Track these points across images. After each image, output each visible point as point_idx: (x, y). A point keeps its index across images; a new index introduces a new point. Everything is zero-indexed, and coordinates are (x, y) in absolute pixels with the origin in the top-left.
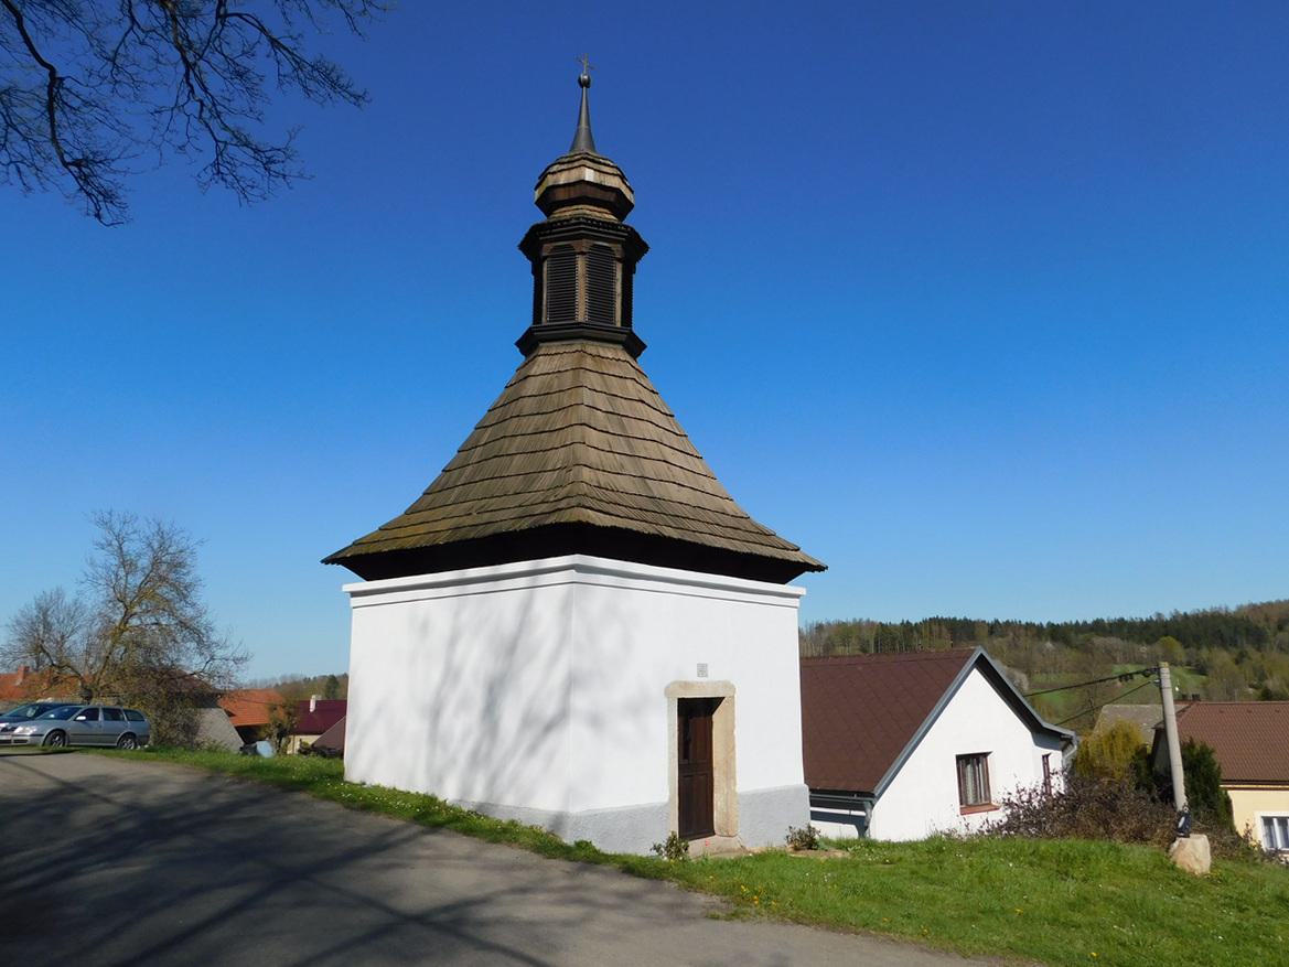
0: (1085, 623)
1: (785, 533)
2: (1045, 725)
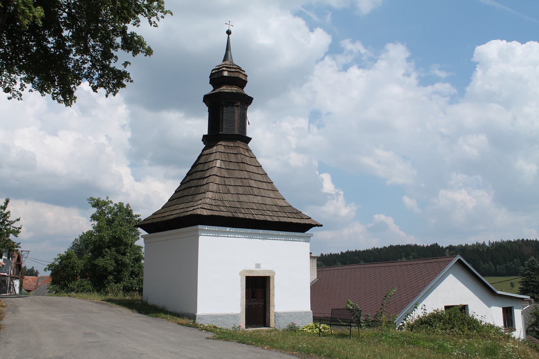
0: (442, 247)
1: (306, 212)
2: (499, 292)
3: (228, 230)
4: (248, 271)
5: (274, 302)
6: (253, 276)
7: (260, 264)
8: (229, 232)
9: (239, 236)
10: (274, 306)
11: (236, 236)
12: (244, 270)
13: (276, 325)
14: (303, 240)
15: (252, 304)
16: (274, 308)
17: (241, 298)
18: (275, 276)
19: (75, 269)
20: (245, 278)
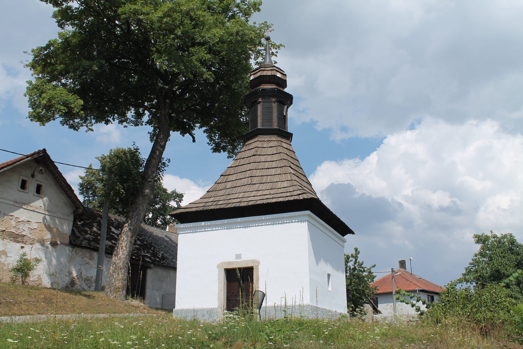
7: (241, 254)
8: (205, 227)
9: (217, 228)
14: (296, 221)
17: (219, 291)
20: (223, 270)
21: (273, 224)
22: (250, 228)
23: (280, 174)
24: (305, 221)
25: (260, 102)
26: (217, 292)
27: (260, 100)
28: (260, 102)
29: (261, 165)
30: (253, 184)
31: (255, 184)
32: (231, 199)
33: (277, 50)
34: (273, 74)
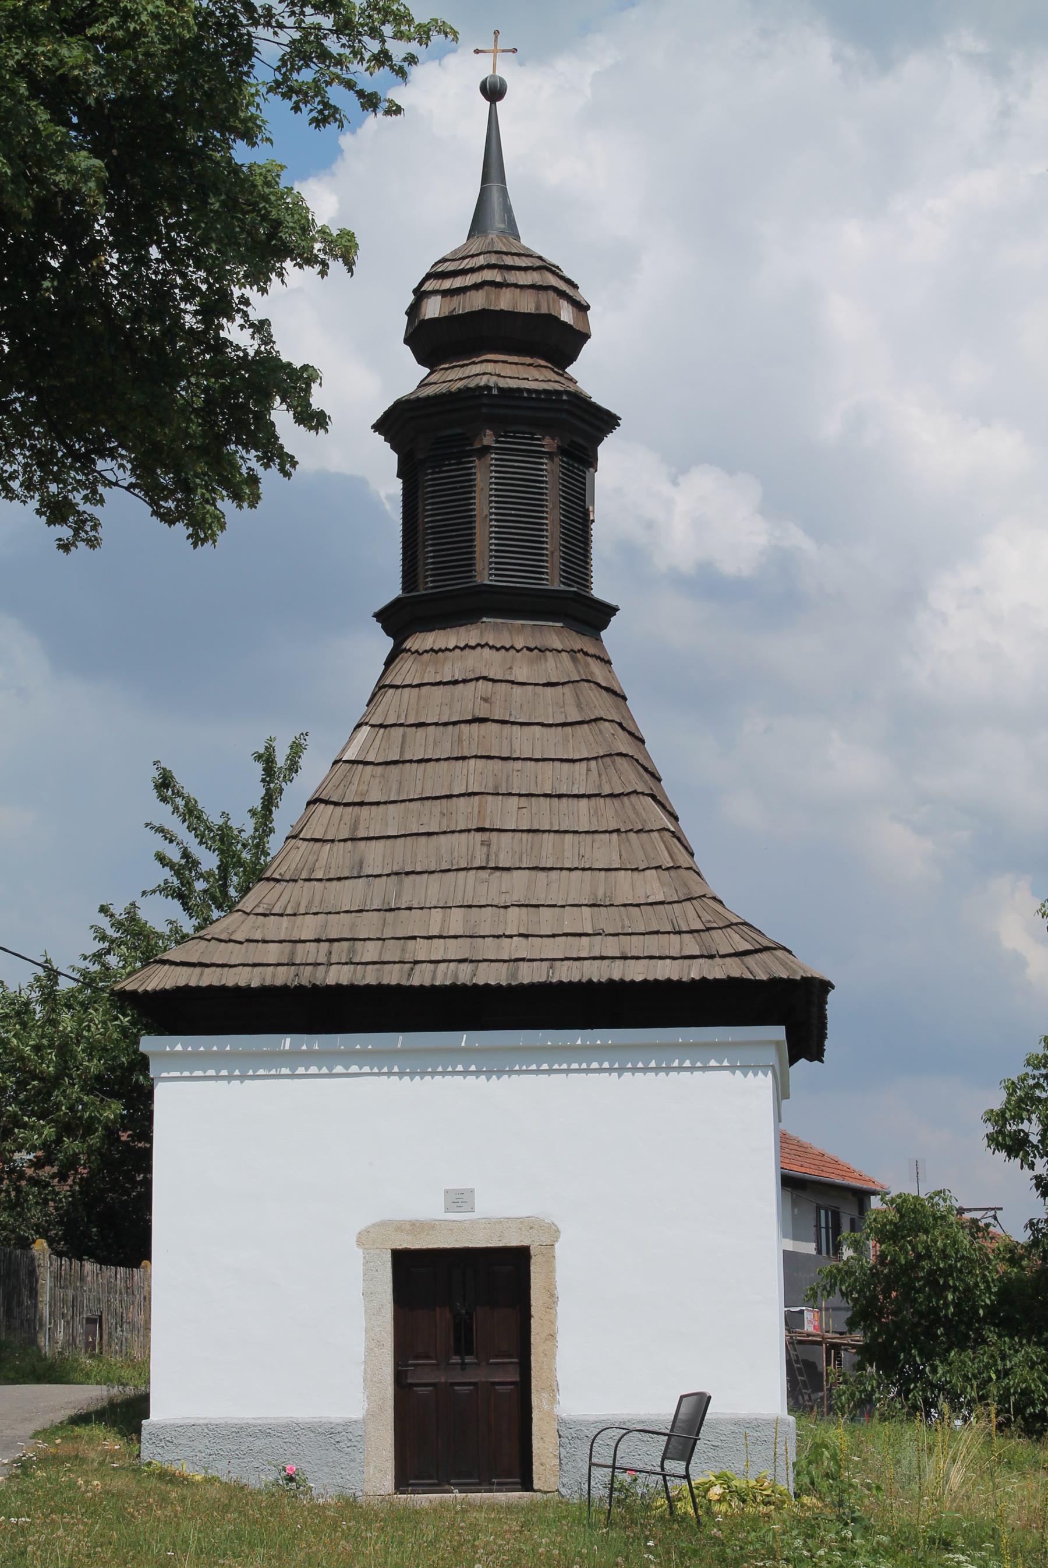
3: (287, 1047)
4: (408, 1227)
5: (552, 1370)
6: (430, 1247)
7: (472, 1191)
8: (294, 1056)
9: (354, 1069)
10: (553, 1390)
11: (334, 1071)
12: (383, 1224)
13: (565, 1480)
14: (726, 1063)
15: (497, 1380)
16: (553, 1401)
17: (369, 1350)
18: (556, 1246)
19: (946, 1287)
20: (388, 1258)
21: (621, 1070)
22: (514, 1077)
23: (618, 831)
24: (764, 1068)
25: (486, 450)
26: (361, 1350)
27: (488, 439)
28: (486, 450)
29: (522, 777)
30: (497, 868)
31: (508, 869)
32: (414, 938)
33: (413, 47)
34: (544, 310)
